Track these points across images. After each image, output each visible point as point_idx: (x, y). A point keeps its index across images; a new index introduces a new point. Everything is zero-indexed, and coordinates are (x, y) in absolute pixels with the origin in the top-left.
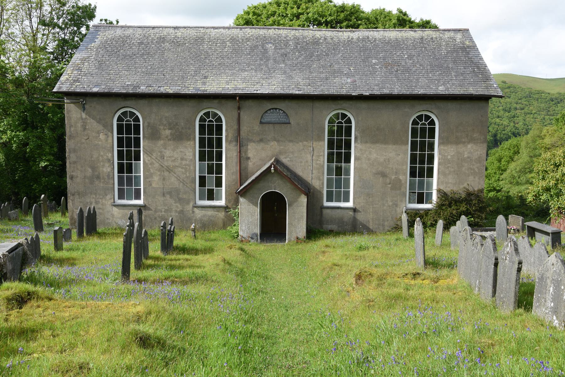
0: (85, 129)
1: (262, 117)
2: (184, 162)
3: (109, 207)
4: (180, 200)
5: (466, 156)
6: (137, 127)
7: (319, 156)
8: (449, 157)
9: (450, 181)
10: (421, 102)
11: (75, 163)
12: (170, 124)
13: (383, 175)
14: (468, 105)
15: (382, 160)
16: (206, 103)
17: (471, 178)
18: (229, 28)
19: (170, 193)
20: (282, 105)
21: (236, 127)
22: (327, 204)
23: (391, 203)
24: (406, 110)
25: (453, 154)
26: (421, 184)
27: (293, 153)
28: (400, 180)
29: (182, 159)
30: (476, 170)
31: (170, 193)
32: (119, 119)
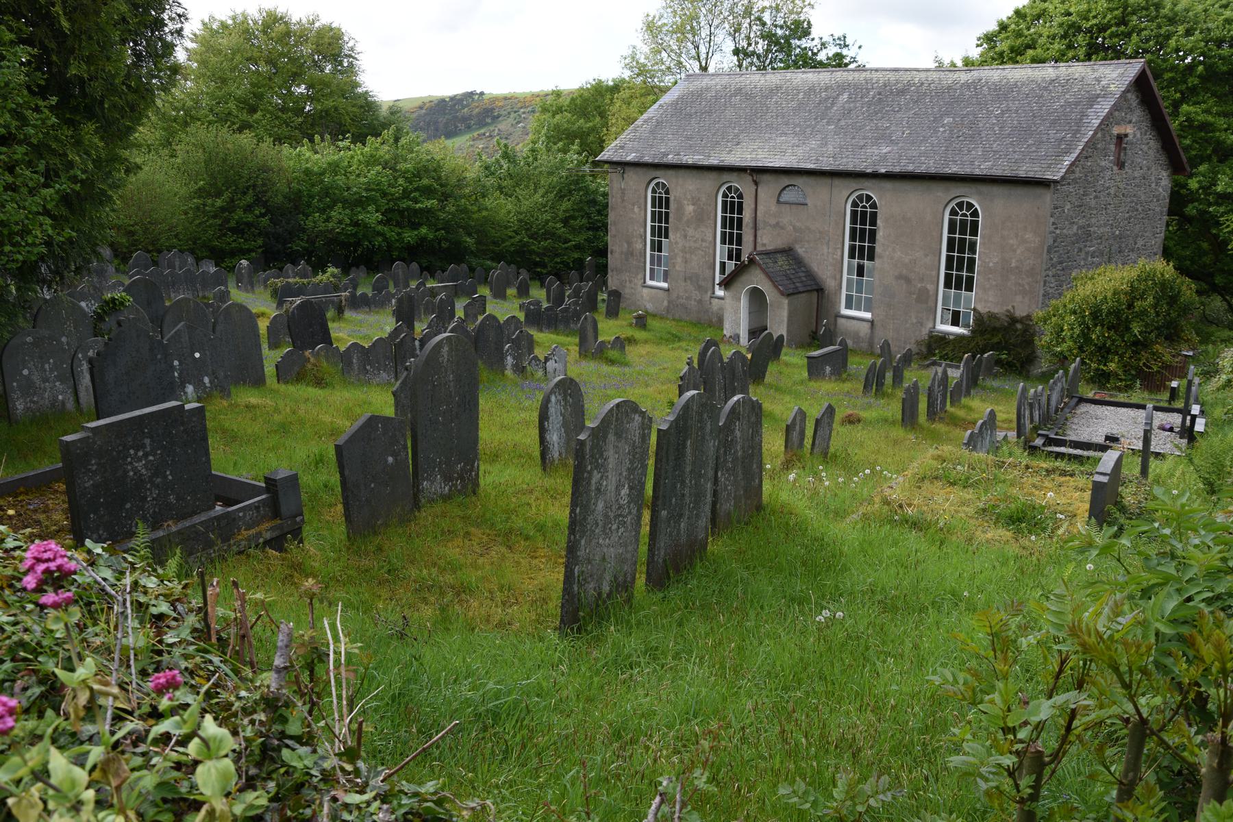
0: (623, 201)
1: (780, 194)
2: (704, 244)
3: (639, 288)
4: (700, 288)
5: (1013, 265)
6: (975, 225)
7: (836, 249)
8: (991, 264)
9: (990, 299)
10: (959, 184)
11: (615, 236)
12: (693, 198)
13: (908, 280)
14: (1020, 191)
15: (907, 261)
16: (725, 176)
17: (1019, 298)
18: (928, 70)
19: (690, 278)
20: (799, 181)
21: (753, 206)
22: (845, 312)
23: (915, 321)
24: (939, 194)
25: (996, 260)
26: (957, 301)
27: (808, 242)
28: (928, 291)
29: (702, 240)
30: (1027, 287)
31: (690, 278)
32: (855, 204)
